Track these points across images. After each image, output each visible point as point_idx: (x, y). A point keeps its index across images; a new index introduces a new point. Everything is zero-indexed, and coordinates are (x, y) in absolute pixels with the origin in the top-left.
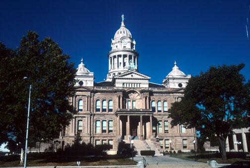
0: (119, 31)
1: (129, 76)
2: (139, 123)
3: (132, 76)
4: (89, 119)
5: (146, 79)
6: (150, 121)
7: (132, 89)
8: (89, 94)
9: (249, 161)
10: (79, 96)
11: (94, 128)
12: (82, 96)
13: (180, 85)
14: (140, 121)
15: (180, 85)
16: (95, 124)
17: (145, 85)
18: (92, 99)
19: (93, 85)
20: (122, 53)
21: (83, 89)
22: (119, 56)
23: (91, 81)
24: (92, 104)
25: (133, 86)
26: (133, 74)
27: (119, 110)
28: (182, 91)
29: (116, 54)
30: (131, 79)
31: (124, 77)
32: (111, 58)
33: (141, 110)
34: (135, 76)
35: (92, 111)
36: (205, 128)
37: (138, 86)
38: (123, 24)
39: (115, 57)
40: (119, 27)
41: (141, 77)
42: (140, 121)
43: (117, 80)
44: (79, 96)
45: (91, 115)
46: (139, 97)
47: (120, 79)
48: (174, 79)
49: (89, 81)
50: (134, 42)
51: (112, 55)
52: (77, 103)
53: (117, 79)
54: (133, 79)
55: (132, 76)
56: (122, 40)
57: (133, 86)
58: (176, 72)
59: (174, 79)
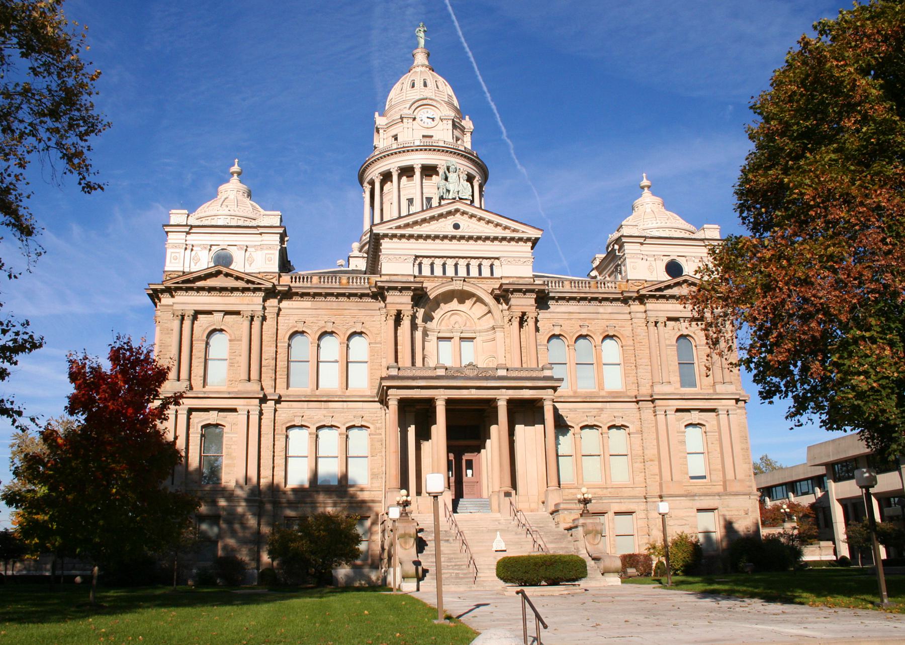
0: (406, 80)
1: (444, 227)
2: (494, 429)
3: (456, 226)
4: (254, 418)
5: (520, 239)
6: (542, 421)
7: (457, 286)
8: (253, 302)
9: (903, 577)
10: (210, 313)
11: (280, 461)
12: (227, 313)
13: (674, 269)
14: (496, 422)
15: (674, 269)
16: (280, 443)
17: (516, 264)
18: (269, 324)
19: (277, 270)
20: (417, 160)
21: (230, 283)
22: (407, 171)
23: (270, 247)
24: (268, 352)
25: (462, 272)
26: (458, 218)
27: (394, 372)
28: (684, 290)
29: (392, 164)
30: (453, 238)
31: (416, 230)
32: (372, 183)
33: (502, 373)
34: (469, 227)
35: (268, 383)
36: (82, 583)
37: (486, 272)
38: (421, 58)
39: (387, 177)
40: (407, 65)
41: (499, 232)
42: (496, 422)
43: (385, 244)
44: (210, 313)
45: (264, 400)
46: (488, 322)
47: (402, 236)
48: (644, 239)
49: (260, 247)
50: (468, 123)
51: (374, 173)
52: (199, 346)
53: (385, 236)
54: (462, 238)
55: (456, 226)
56: (419, 111)
57: (462, 272)
58: (649, 214)
59: (644, 239)
